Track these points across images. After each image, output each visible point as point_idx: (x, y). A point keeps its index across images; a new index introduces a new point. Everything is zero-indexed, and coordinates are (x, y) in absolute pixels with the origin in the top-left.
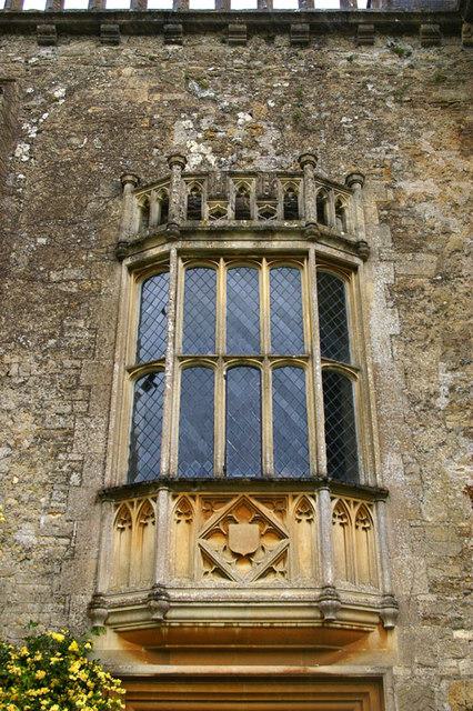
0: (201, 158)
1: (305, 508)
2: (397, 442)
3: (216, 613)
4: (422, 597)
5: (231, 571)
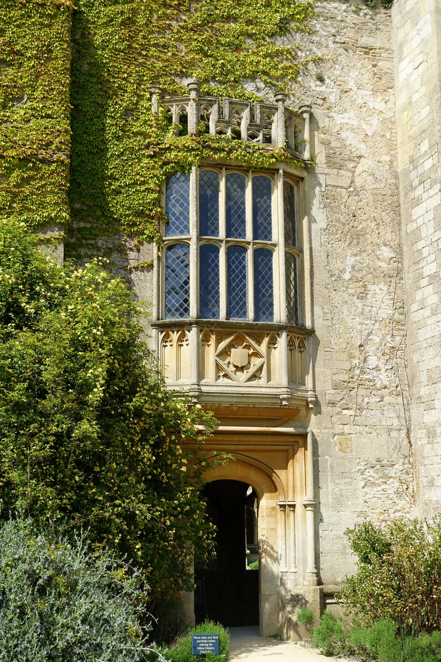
1: (273, 343)
2: (320, 299)
3: (226, 400)
4: (328, 392)
5: (232, 375)
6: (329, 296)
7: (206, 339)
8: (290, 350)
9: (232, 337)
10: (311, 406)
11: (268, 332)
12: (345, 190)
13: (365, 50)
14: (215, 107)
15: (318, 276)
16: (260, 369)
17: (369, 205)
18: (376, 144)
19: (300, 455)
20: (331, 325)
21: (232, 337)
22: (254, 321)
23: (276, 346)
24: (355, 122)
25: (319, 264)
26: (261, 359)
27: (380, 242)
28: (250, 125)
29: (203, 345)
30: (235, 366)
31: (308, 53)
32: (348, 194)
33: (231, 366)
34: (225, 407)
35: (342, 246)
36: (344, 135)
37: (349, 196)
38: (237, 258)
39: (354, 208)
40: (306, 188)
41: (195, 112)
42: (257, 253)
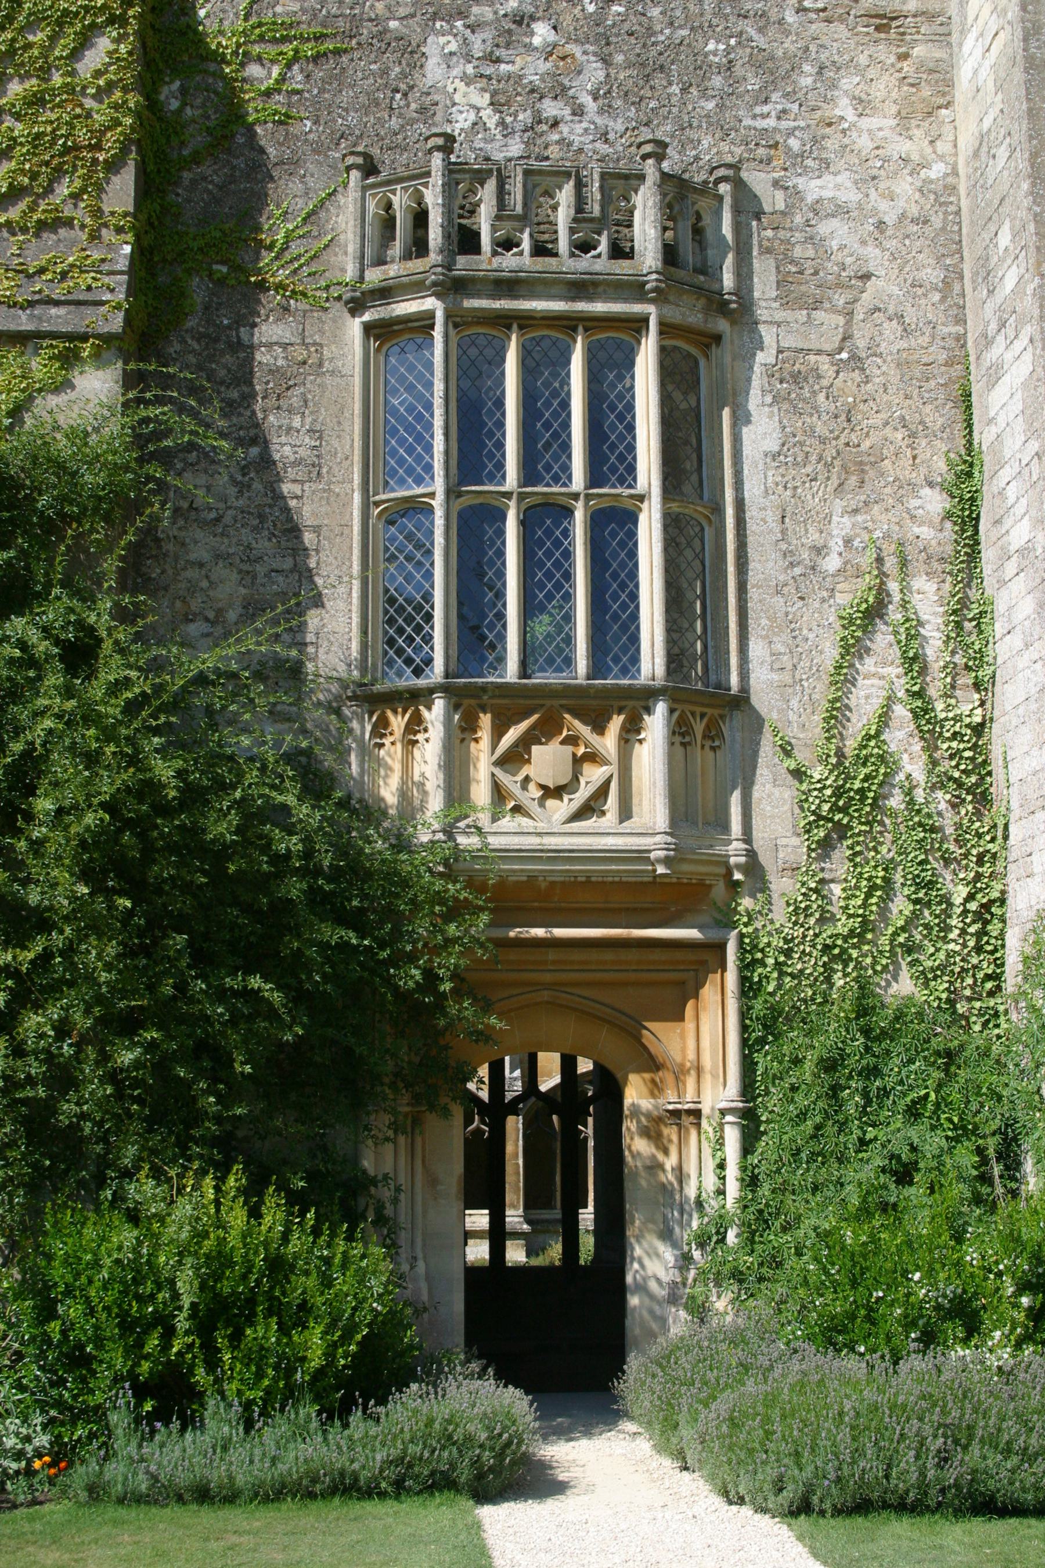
0: (472, 117)
1: (632, 730)
5: (534, 808)
6: (787, 614)
7: (469, 727)
8: (684, 745)
9: (536, 717)
10: (738, 876)
11: (623, 703)
12: (827, 359)
13: (878, 21)
14: (491, 185)
15: (758, 566)
16: (603, 791)
17: (890, 391)
18: (907, 242)
19: (709, 992)
20: (791, 681)
21: (536, 717)
22: (588, 677)
23: (641, 737)
24: (850, 196)
25: (761, 540)
26: (605, 768)
27: (917, 477)
28: (575, 220)
29: (463, 740)
30: (543, 787)
31: (733, 42)
32: (835, 368)
33: (532, 786)
34: (517, 882)
35: (820, 494)
36: (824, 228)
37: (838, 372)
38: (549, 533)
39: (851, 400)
40: (728, 359)
41: (440, 201)
42: (598, 521)
